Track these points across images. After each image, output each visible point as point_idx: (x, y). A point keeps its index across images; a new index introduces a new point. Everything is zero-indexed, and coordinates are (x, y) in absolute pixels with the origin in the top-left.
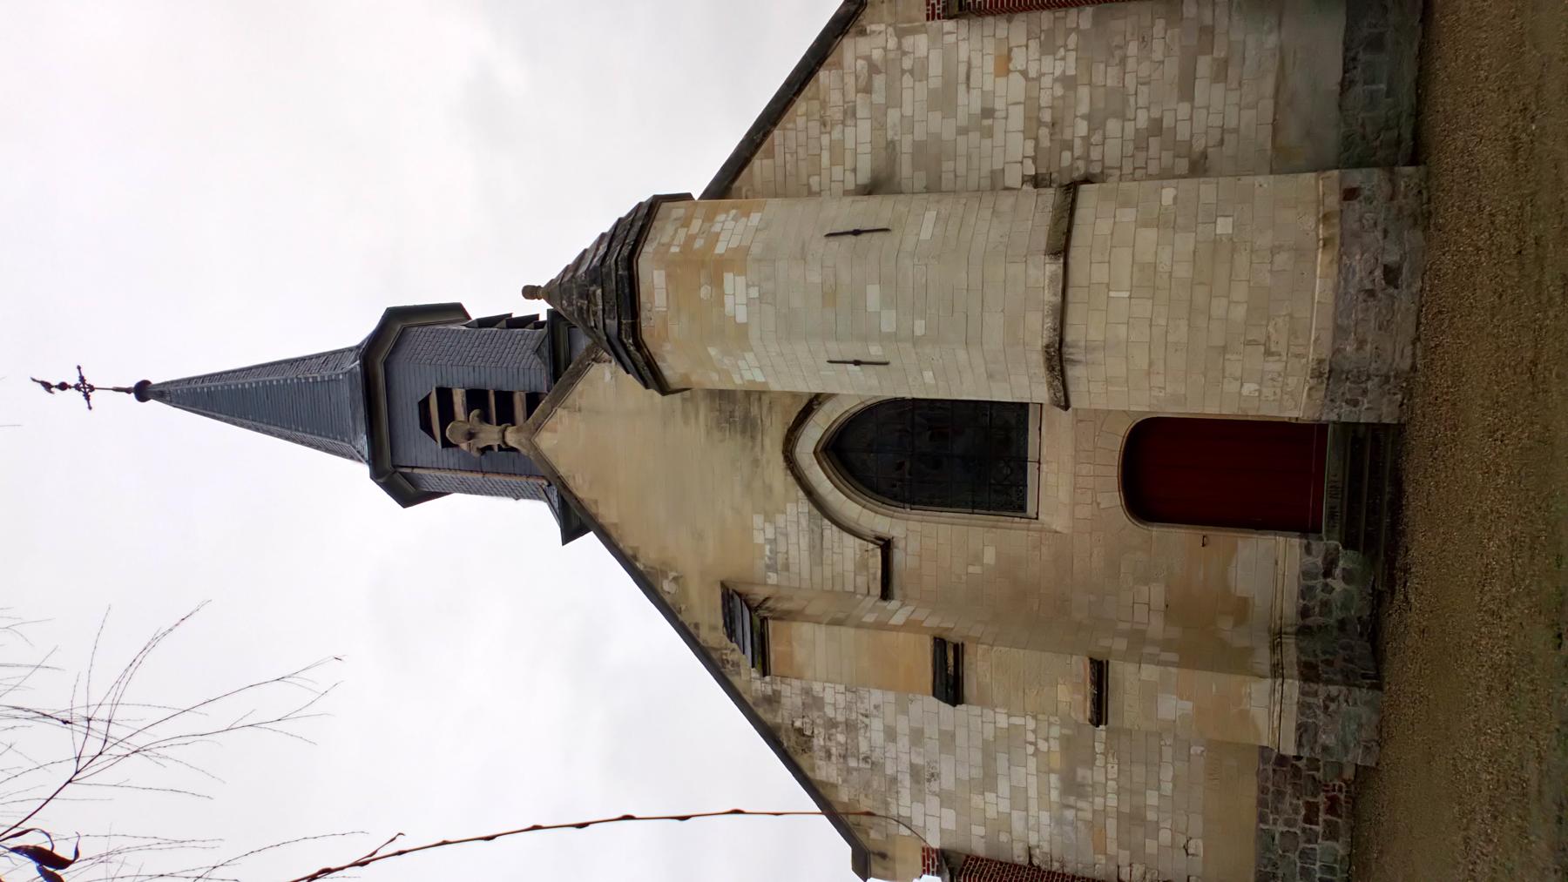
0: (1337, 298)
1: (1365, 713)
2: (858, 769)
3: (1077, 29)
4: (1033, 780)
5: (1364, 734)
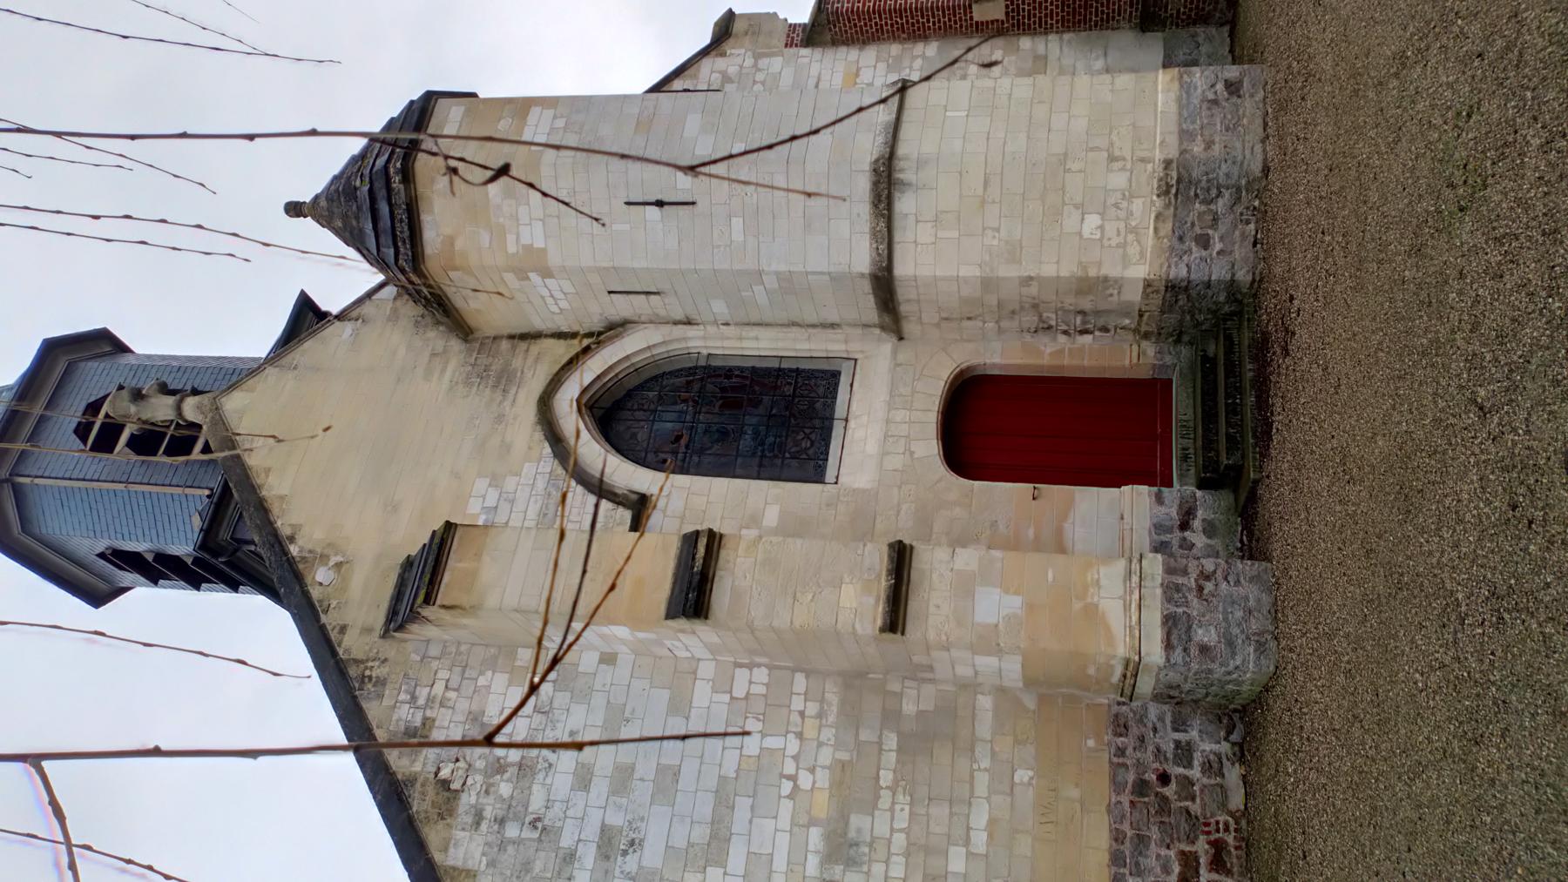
0: (1180, 107)
1: (1251, 592)
2: (517, 842)
3: (923, 56)
4: (783, 840)
5: (1254, 626)
